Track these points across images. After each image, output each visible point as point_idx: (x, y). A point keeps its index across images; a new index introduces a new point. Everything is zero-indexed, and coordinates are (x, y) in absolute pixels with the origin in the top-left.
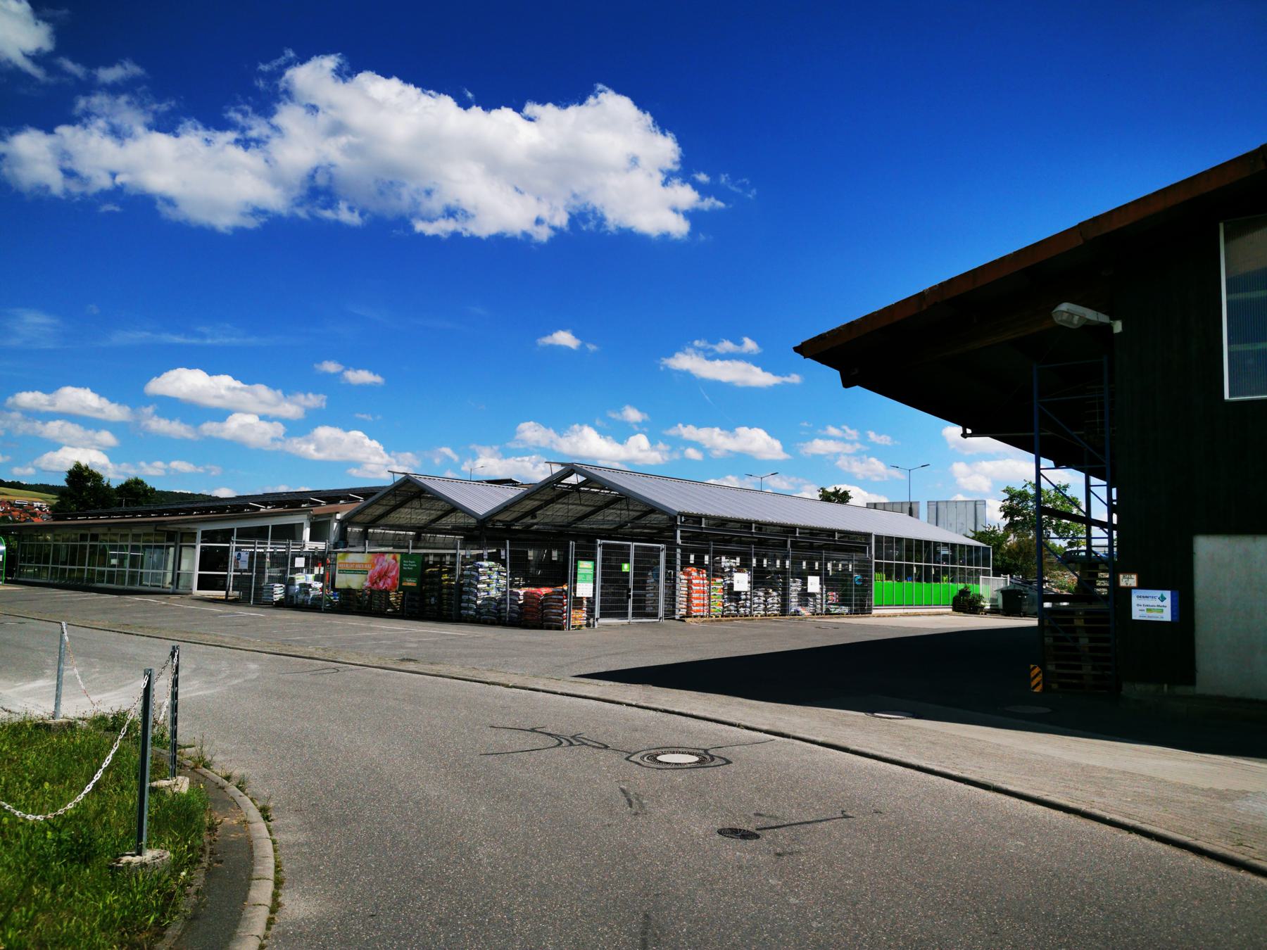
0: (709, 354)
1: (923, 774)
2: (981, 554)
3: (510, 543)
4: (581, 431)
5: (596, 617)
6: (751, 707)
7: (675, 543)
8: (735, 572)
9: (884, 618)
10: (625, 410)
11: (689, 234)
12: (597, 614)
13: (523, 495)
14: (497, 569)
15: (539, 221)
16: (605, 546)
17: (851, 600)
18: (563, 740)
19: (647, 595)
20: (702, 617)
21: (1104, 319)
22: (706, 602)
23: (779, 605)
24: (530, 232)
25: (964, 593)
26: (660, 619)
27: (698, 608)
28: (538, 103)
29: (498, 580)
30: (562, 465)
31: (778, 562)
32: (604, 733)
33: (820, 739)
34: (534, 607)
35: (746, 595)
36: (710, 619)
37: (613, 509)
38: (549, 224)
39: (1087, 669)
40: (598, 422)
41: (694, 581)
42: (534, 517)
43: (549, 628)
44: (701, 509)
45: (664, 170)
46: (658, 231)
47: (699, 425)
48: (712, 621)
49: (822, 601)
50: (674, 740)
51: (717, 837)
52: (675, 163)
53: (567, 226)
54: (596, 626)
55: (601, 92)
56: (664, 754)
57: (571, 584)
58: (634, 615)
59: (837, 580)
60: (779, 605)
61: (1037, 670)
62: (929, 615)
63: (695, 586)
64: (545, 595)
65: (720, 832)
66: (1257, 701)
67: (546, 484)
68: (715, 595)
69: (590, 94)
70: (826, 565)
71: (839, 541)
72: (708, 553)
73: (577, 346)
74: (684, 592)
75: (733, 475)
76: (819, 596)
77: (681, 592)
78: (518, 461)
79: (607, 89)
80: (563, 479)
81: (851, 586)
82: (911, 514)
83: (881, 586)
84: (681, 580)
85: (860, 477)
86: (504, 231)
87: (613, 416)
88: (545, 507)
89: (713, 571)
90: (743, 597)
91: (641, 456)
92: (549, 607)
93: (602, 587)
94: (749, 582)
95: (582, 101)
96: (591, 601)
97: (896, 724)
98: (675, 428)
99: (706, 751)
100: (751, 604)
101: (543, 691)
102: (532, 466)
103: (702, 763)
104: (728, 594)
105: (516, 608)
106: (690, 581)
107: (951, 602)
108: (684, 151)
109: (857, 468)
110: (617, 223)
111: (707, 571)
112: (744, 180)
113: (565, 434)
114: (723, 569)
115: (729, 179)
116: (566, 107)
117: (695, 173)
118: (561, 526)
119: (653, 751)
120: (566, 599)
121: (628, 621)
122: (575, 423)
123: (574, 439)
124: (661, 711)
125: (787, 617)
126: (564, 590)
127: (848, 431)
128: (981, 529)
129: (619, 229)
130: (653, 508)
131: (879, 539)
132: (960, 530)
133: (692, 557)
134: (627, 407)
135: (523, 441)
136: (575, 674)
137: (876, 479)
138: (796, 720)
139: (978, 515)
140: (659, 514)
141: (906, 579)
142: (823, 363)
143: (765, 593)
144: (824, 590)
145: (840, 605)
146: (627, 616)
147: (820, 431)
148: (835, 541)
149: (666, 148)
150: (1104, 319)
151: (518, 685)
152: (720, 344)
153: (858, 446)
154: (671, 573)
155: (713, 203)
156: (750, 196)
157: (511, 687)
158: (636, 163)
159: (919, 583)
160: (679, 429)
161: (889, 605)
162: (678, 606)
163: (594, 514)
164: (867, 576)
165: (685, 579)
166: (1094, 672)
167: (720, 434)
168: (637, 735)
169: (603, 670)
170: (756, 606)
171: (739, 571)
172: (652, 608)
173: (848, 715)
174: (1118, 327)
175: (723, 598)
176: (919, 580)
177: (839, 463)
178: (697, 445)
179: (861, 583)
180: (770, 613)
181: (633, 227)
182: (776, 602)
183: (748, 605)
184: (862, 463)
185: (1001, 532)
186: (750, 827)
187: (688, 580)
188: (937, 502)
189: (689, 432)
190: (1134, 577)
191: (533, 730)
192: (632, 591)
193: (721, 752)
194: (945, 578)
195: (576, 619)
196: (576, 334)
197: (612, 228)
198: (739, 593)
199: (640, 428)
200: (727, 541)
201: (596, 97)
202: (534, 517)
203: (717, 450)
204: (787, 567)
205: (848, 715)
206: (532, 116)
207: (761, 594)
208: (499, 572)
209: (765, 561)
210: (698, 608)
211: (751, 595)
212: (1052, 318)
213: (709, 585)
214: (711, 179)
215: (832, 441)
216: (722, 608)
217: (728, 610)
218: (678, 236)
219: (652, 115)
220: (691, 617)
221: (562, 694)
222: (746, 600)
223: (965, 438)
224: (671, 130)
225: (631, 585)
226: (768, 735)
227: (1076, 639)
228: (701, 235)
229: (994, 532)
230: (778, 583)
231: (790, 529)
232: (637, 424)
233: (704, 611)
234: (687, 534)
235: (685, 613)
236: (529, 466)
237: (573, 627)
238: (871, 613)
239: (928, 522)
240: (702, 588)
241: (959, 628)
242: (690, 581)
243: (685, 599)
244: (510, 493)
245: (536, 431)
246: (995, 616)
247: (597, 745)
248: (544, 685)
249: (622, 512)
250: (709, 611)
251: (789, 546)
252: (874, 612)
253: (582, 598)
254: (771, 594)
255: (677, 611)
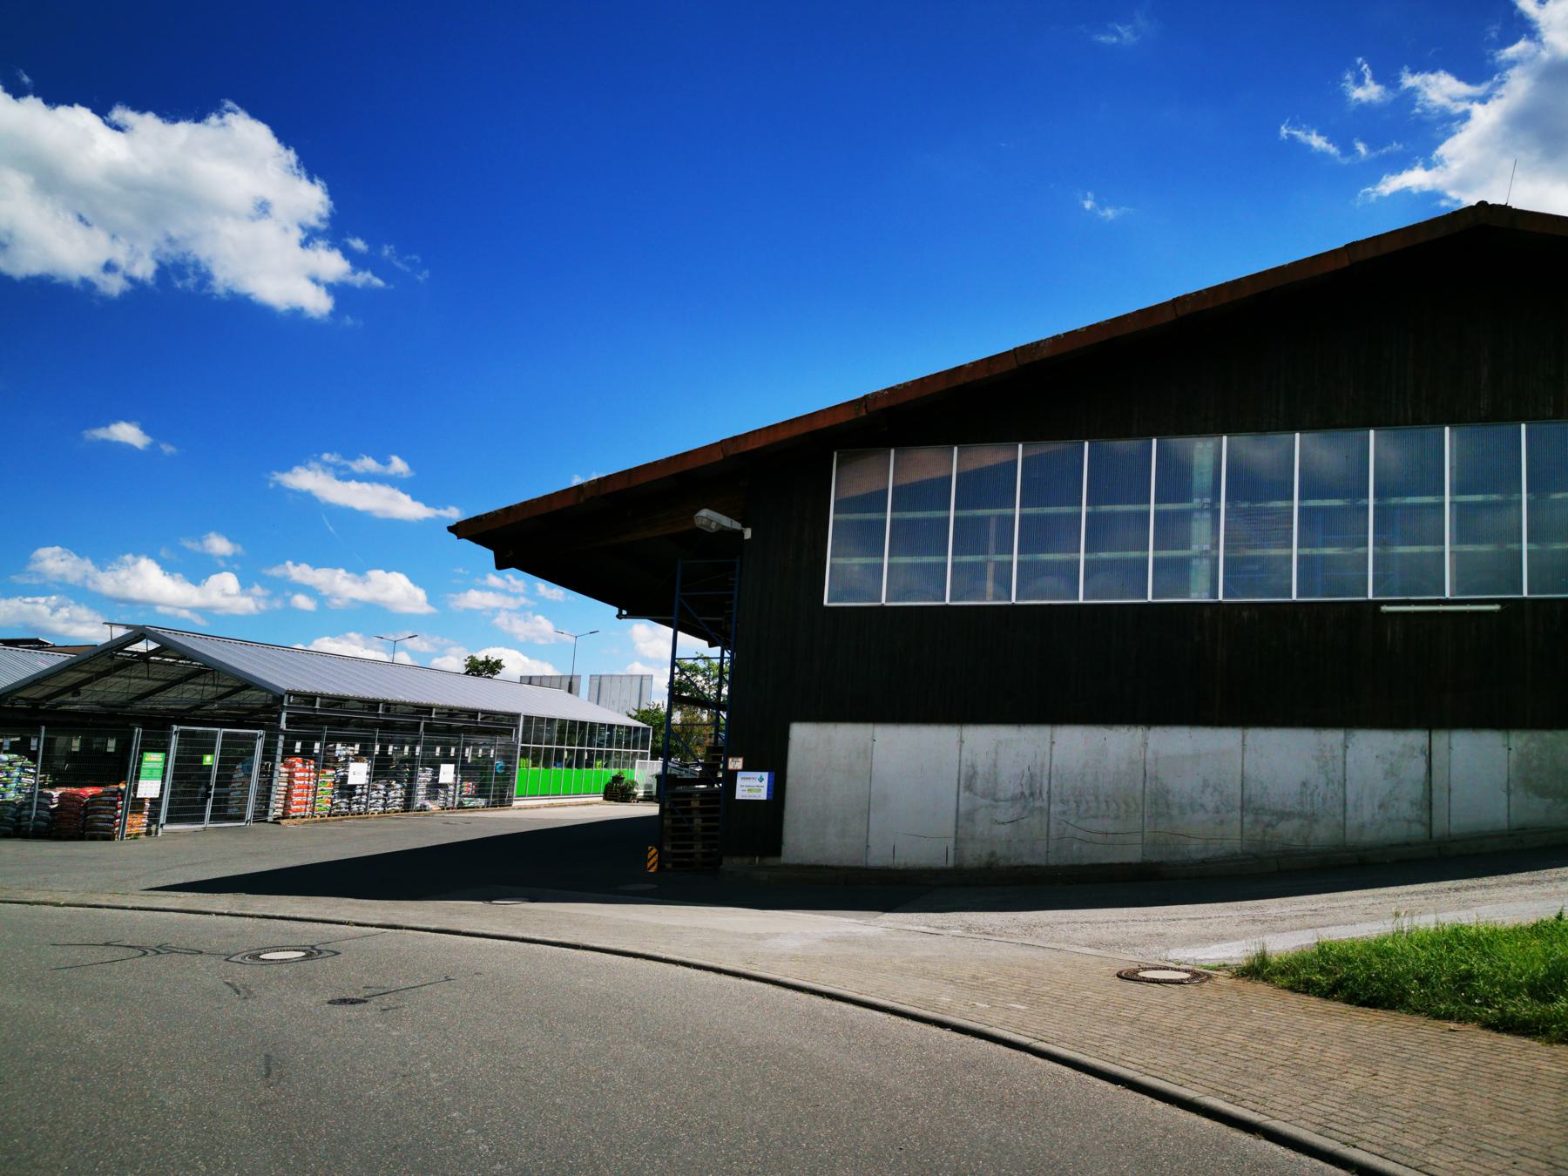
0: (342, 473)
1: (525, 944)
2: (640, 734)
3: (45, 730)
4: (135, 563)
5: (161, 822)
6: (362, 906)
7: (278, 728)
8: (352, 761)
9: (526, 811)
10: (208, 538)
11: (332, 314)
12: (162, 819)
13: (65, 666)
14: (20, 763)
15: (109, 267)
16: (182, 734)
17: (489, 791)
18: (147, 951)
19: (232, 794)
20: (303, 817)
21: (737, 526)
22: (309, 799)
23: (402, 799)
24: (95, 280)
25: (617, 779)
26: (247, 822)
27: (298, 807)
28: (133, 109)
29: (19, 778)
30: (128, 627)
31: (407, 749)
32: (195, 941)
33: (433, 926)
34: (72, 812)
35: (362, 788)
36: (314, 819)
37: (192, 684)
38: (124, 272)
39: (698, 847)
40: (163, 553)
41: (297, 775)
42: (77, 693)
43: (93, 838)
44: (317, 686)
45: (306, 227)
46: (288, 304)
47: (316, 565)
48: (316, 822)
49: (455, 793)
50: (278, 940)
51: (327, 1006)
52: (321, 220)
53: (152, 279)
54: (160, 834)
55: (229, 111)
56: (265, 953)
57: (131, 783)
58: (213, 819)
59: (476, 768)
60: (402, 799)
61: (654, 851)
62: (577, 805)
63: (298, 780)
64: (91, 797)
65: (329, 1003)
66: (827, 867)
67: (102, 652)
68: (322, 790)
69: (212, 111)
70: (464, 750)
71: (481, 723)
72: (319, 739)
73: (146, 446)
74: (283, 789)
75: (357, 632)
76: (452, 787)
77: (279, 788)
78: (25, 603)
79: (238, 108)
80: (128, 646)
81: (491, 774)
82: (570, 691)
83: (525, 772)
84: (280, 773)
85: (521, 638)
86: (52, 274)
87: (188, 545)
88: (96, 680)
89: (323, 762)
90: (359, 791)
91: (225, 602)
92: (95, 812)
93: (173, 786)
94: (368, 774)
95: (199, 117)
96: (156, 802)
97: (511, 908)
98: (282, 566)
99: (313, 947)
100: (367, 800)
101: (108, 907)
102: (49, 610)
103: (309, 956)
104: (339, 789)
105: (45, 814)
106: (291, 775)
107: (602, 790)
108: (336, 206)
109: (520, 628)
110: (227, 285)
111: (315, 761)
112: (414, 257)
113: (109, 568)
114: (337, 758)
115: (394, 252)
116: (175, 121)
117: (350, 237)
118: (112, 706)
119: (254, 952)
120: (122, 800)
121: (204, 826)
122: (127, 553)
123: (123, 575)
124: (258, 917)
125: (410, 813)
126: (119, 790)
127: (513, 581)
128: (644, 707)
129: (231, 293)
130: (247, 684)
131: (528, 719)
132: (623, 708)
133: (298, 745)
134: (212, 535)
135: (38, 574)
136: (145, 887)
137: (541, 642)
138: (411, 914)
139: (643, 691)
140: (256, 690)
141: (555, 765)
142: (477, 543)
143: (387, 786)
144: (459, 779)
145: (475, 797)
146: (204, 820)
147: (478, 580)
148: (477, 723)
149: (312, 199)
150: (737, 526)
151: (72, 902)
152: (358, 461)
153: (523, 600)
154: (268, 764)
155: (368, 279)
156: (420, 278)
157: (63, 905)
158: (266, 212)
159: (569, 770)
160: (287, 568)
161: (533, 796)
162: (272, 805)
163: (164, 690)
164: (510, 763)
165: (286, 773)
166: (704, 850)
167: (345, 578)
168: (234, 940)
169: (161, 885)
170: (373, 801)
171: (357, 761)
172: (236, 810)
173: (465, 905)
174: (748, 534)
175: (333, 794)
176: (569, 766)
177: (497, 620)
178: (310, 591)
179: (502, 771)
180: (390, 809)
181: (251, 294)
182: (399, 795)
183: (364, 800)
184: (526, 621)
185: (664, 710)
186: (360, 996)
187: (289, 773)
188: (601, 676)
189: (300, 573)
190: (741, 760)
191: (107, 944)
192: (213, 789)
193: (330, 947)
194: (599, 763)
195: (132, 826)
196: (146, 429)
197: (220, 290)
198: (353, 787)
199: (228, 564)
200: (342, 723)
201: (221, 116)
202: (77, 693)
203: (338, 598)
204: (417, 754)
205: (465, 905)
206: (121, 123)
207: (382, 787)
208: (22, 768)
209: (391, 748)
210: (298, 807)
211: (368, 789)
212: (693, 520)
213: (317, 779)
214: (369, 248)
215: (491, 593)
216: (330, 805)
217: (337, 808)
218: (316, 315)
219: (297, 152)
220: (288, 818)
221: (133, 909)
222: (361, 795)
223: (620, 619)
224: (321, 177)
225: (213, 781)
226: (380, 929)
227: (691, 820)
228: (348, 317)
229: (658, 709)
230: (404, 773)
231: (426, 710)
232: (224, 558)
233: (305, 811)
234: (291, 716)
235: (280, 814)
236: (46, 611)
237: (128, 835)
238: (510, 805)
239: (589, 700)
240: (307, 782)
241: (586, 819)
242: (291, 775)
243: (283, 797)
244: (42, 662)
245: (62, 560)
246: (647, 803)
247: (190, 952)
248: (108, 900)
249: (205, 687)
250: (313, 811)
251: (422, 729)
252: (515, 804)
253: (143, 799)
254: (393, 786)
255: (271, 811)
